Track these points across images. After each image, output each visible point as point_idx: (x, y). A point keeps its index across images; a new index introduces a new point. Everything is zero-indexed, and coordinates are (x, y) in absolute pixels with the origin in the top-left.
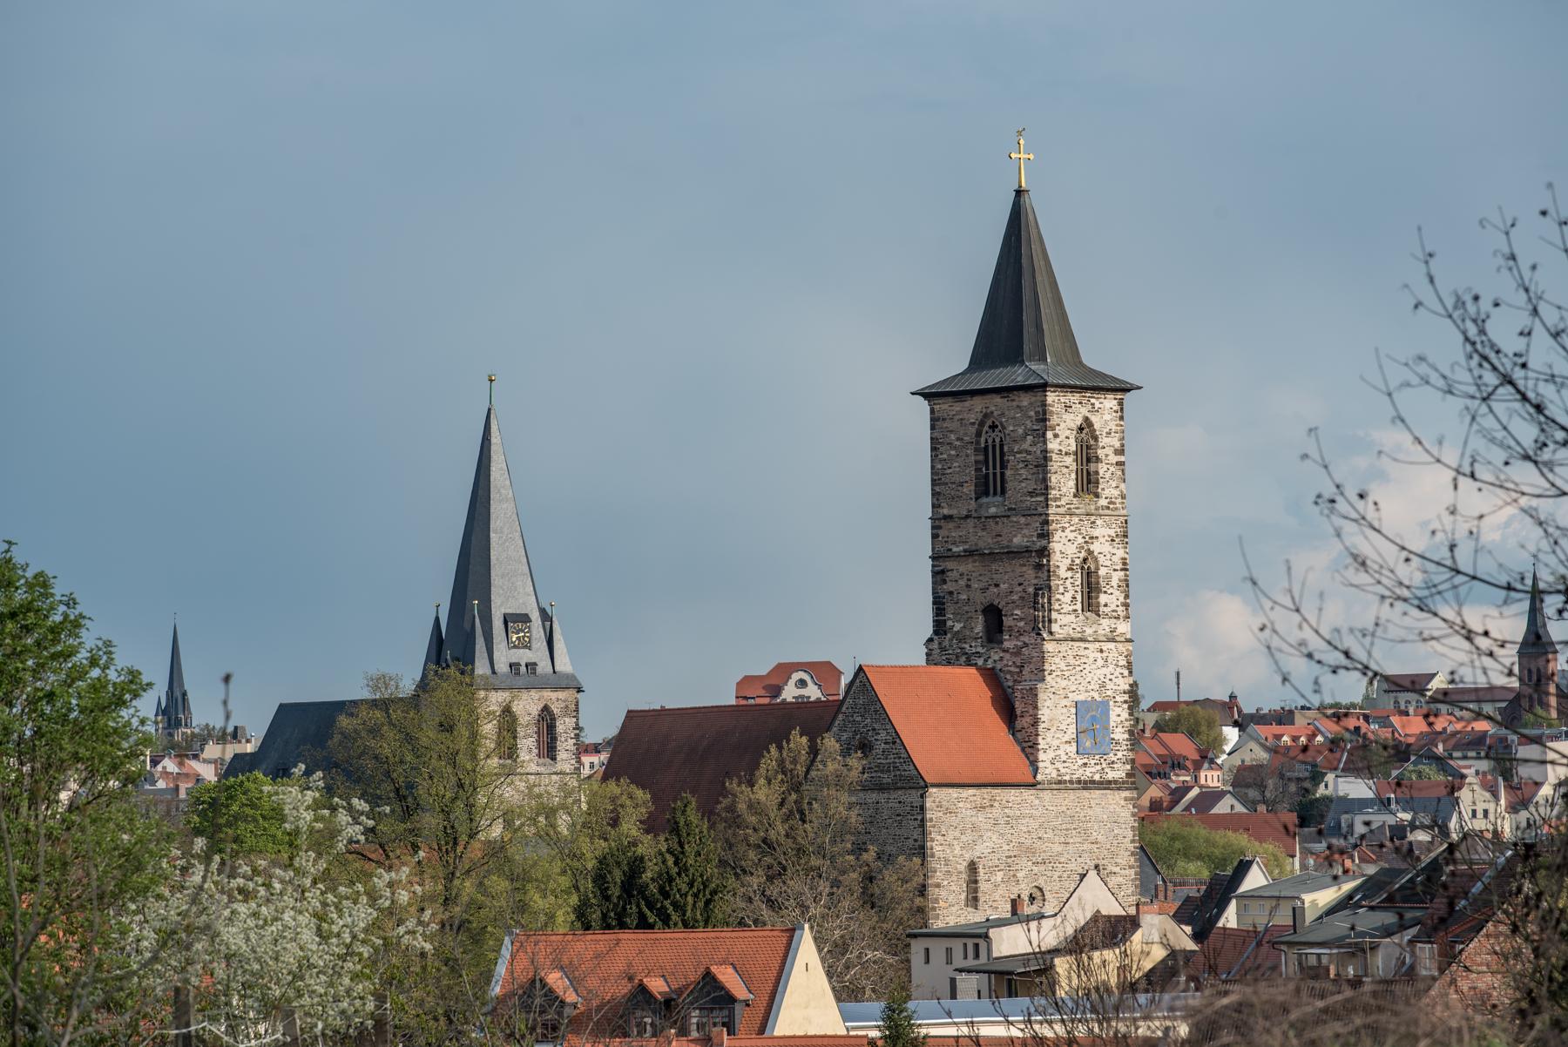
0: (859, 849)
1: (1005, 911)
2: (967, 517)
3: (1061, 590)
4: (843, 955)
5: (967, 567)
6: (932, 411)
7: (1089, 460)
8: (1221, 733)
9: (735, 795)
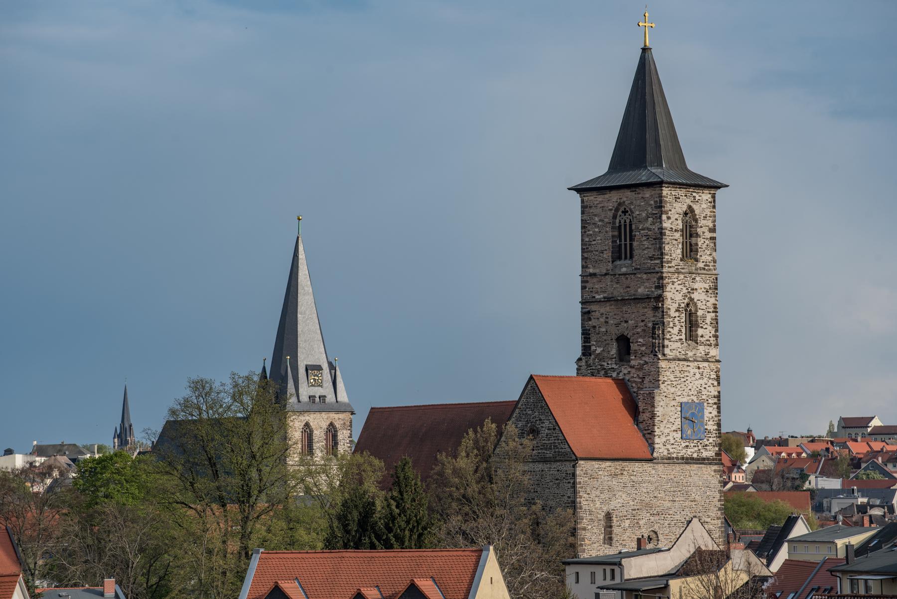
0: (530, 503)
1: (632, 546)
2: (606, 274)
3: (671, 325)
4: (519, 574)
5: (606, 309)
6: (582, 201)
7: (691, 236)
8: (744, 451)
9: (443, 464)
